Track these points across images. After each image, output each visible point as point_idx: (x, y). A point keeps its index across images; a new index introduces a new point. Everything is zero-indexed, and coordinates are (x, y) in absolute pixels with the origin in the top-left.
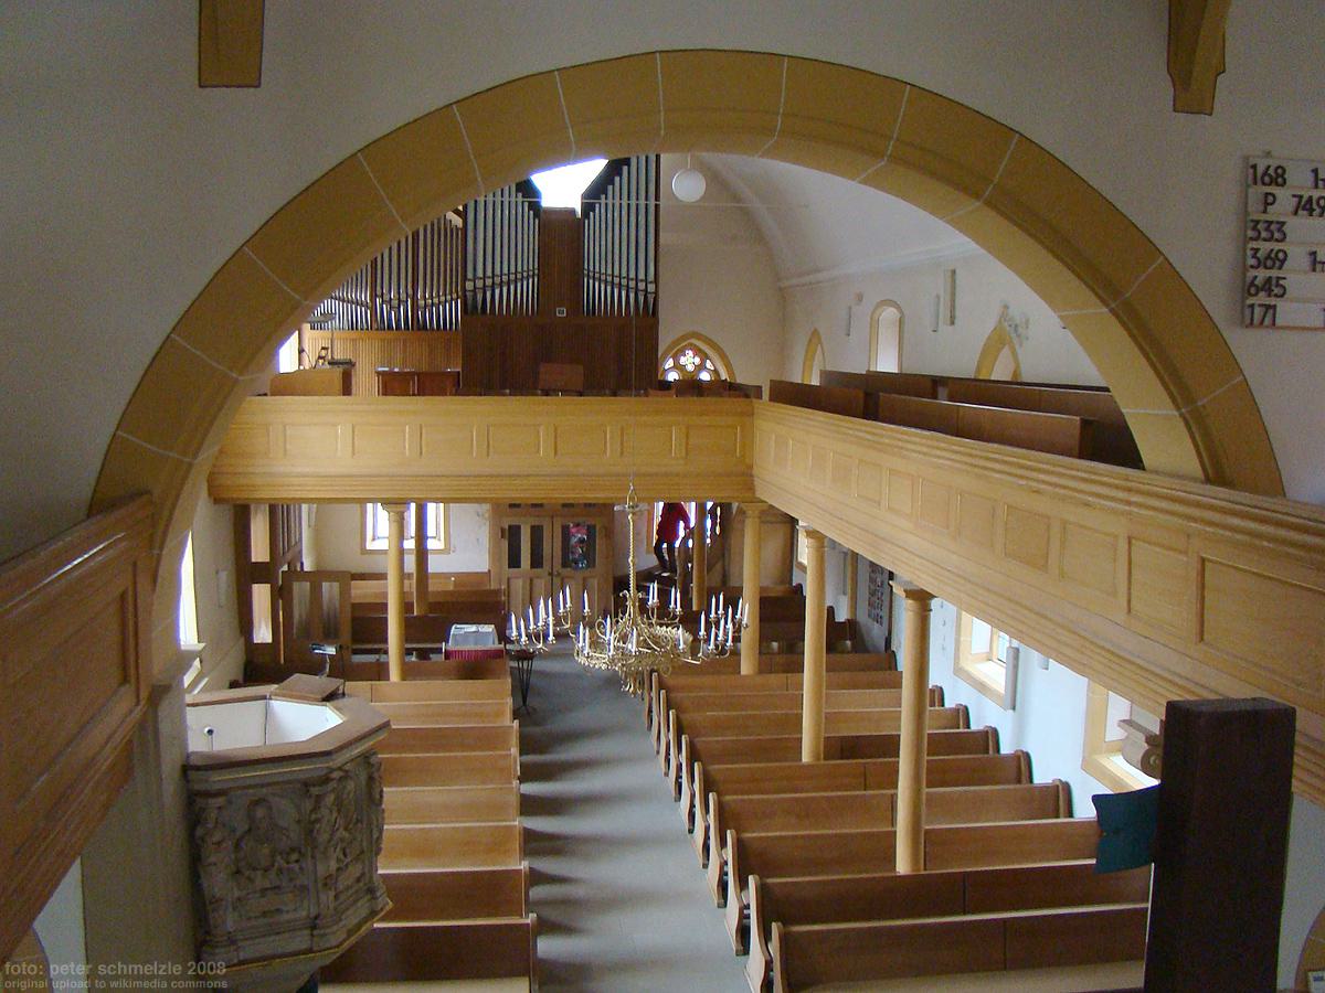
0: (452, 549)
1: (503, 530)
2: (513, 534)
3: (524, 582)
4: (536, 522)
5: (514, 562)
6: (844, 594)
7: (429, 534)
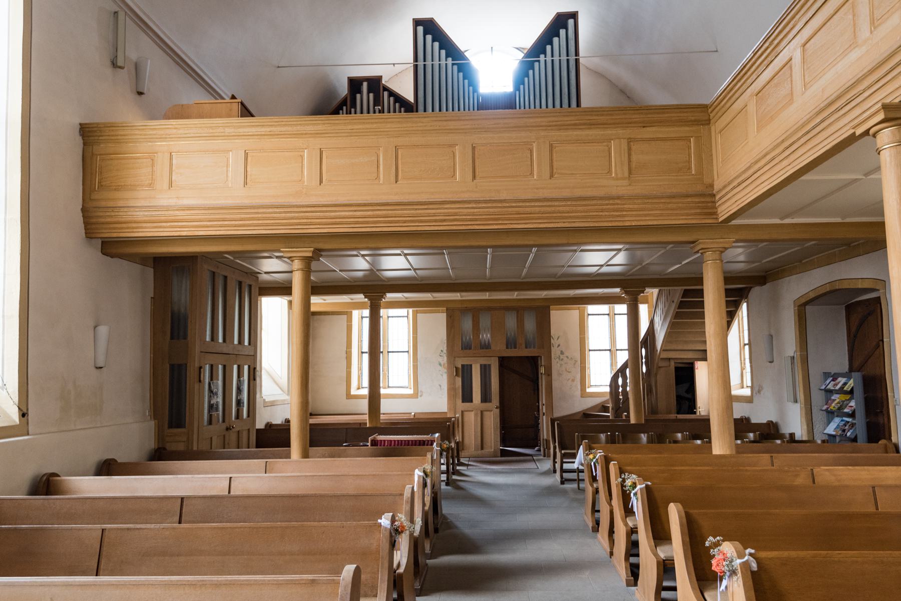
0: (419, 394)
1: (457, 369)
2: (465, 373)
3: (476, 415)
4: (484, 361)
5: (467, 397)
6: (796, 401)
7: (368, 319)
